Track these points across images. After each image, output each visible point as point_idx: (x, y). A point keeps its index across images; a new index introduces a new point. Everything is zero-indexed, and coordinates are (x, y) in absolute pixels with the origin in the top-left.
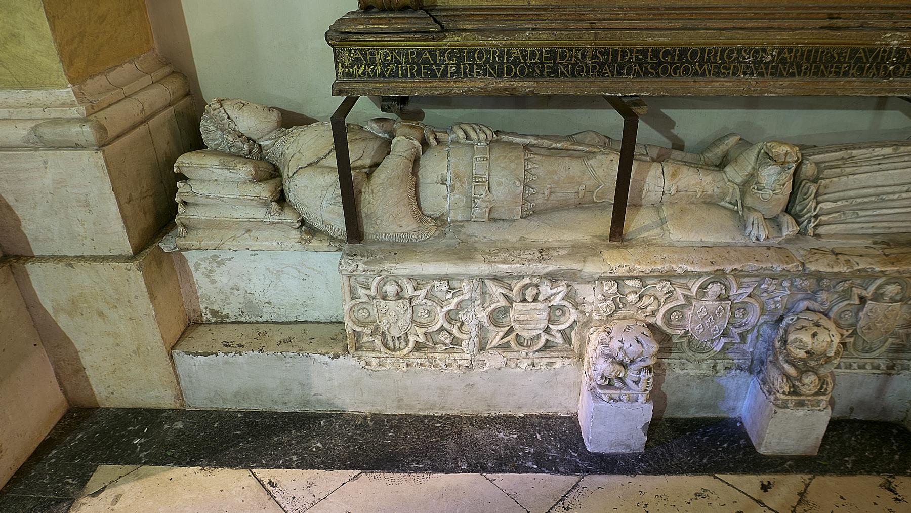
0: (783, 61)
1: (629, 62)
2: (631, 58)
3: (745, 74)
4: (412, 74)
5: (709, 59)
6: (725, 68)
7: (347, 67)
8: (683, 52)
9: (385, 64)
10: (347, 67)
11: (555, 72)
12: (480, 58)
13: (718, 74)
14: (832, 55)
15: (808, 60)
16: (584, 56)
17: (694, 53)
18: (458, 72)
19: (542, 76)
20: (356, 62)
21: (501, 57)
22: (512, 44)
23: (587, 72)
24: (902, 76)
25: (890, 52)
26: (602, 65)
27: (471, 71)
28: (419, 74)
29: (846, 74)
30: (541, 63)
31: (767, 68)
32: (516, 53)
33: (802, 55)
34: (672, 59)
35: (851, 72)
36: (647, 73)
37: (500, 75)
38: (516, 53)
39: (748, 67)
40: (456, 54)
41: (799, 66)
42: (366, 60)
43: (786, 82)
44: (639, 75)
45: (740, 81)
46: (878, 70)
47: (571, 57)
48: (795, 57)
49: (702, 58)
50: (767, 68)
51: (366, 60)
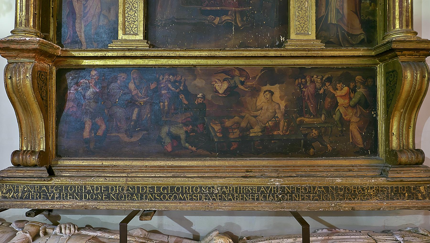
0: (224, 193)
1: (146, 193)
2: (146, 191)
3: (206, 199)
4: (36, 197)
5: (186, 191)
6: (195, 196)
7: (4, 194)
8: (172, 188)
9: (23, 192)
10: (4, 194)
11: (108, 197)
12: (71, 190)
13: (192, 199)
14: (248, 190)
15: (237, 192)
16: (123, 190)
17: (178, 189)
18: (59, 197)
19: (102, 199)
20: (9, 191)
21: (81, 190)
22: (85, 184)
23: (125, 198)
24: (287, 200)
25: (277, 188)
26: (132, 195)
27: (66, 196)
28: (40, 198)
29: (258, 199)
30: (101, 193)
31: (216, 196)
32: (89, 188)
33: (233, 190)
34: (168, 191)
35: (260, 198)
36: (155, 199)
37: (81, 199)
38: (89, 188)
39: (207, 196)
40: (59, 188)
41: (233, 195)
42: (14, 190)
43: (227, 203)
44: (151, 200)
45: (203, 203)
46: (274, 197)
47: (116, 190)
48: (230, 191)
49: (182, 191)
50: (216, 196)
51: (14, 190)
